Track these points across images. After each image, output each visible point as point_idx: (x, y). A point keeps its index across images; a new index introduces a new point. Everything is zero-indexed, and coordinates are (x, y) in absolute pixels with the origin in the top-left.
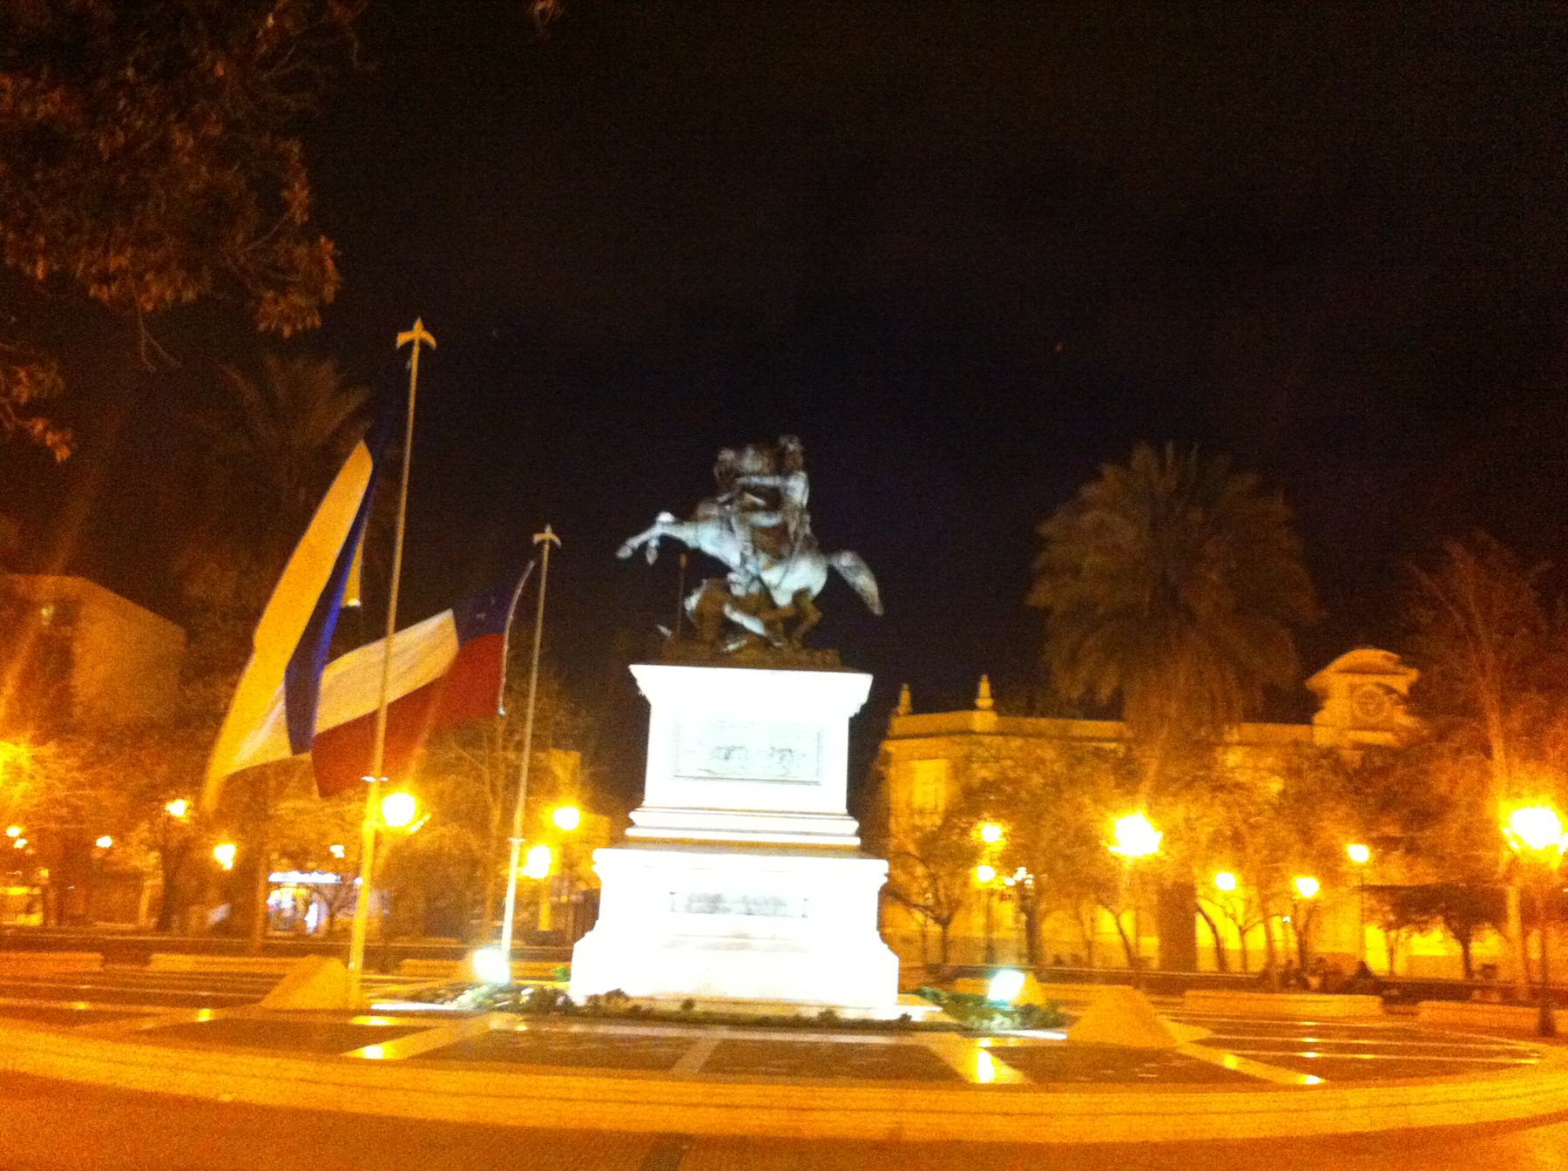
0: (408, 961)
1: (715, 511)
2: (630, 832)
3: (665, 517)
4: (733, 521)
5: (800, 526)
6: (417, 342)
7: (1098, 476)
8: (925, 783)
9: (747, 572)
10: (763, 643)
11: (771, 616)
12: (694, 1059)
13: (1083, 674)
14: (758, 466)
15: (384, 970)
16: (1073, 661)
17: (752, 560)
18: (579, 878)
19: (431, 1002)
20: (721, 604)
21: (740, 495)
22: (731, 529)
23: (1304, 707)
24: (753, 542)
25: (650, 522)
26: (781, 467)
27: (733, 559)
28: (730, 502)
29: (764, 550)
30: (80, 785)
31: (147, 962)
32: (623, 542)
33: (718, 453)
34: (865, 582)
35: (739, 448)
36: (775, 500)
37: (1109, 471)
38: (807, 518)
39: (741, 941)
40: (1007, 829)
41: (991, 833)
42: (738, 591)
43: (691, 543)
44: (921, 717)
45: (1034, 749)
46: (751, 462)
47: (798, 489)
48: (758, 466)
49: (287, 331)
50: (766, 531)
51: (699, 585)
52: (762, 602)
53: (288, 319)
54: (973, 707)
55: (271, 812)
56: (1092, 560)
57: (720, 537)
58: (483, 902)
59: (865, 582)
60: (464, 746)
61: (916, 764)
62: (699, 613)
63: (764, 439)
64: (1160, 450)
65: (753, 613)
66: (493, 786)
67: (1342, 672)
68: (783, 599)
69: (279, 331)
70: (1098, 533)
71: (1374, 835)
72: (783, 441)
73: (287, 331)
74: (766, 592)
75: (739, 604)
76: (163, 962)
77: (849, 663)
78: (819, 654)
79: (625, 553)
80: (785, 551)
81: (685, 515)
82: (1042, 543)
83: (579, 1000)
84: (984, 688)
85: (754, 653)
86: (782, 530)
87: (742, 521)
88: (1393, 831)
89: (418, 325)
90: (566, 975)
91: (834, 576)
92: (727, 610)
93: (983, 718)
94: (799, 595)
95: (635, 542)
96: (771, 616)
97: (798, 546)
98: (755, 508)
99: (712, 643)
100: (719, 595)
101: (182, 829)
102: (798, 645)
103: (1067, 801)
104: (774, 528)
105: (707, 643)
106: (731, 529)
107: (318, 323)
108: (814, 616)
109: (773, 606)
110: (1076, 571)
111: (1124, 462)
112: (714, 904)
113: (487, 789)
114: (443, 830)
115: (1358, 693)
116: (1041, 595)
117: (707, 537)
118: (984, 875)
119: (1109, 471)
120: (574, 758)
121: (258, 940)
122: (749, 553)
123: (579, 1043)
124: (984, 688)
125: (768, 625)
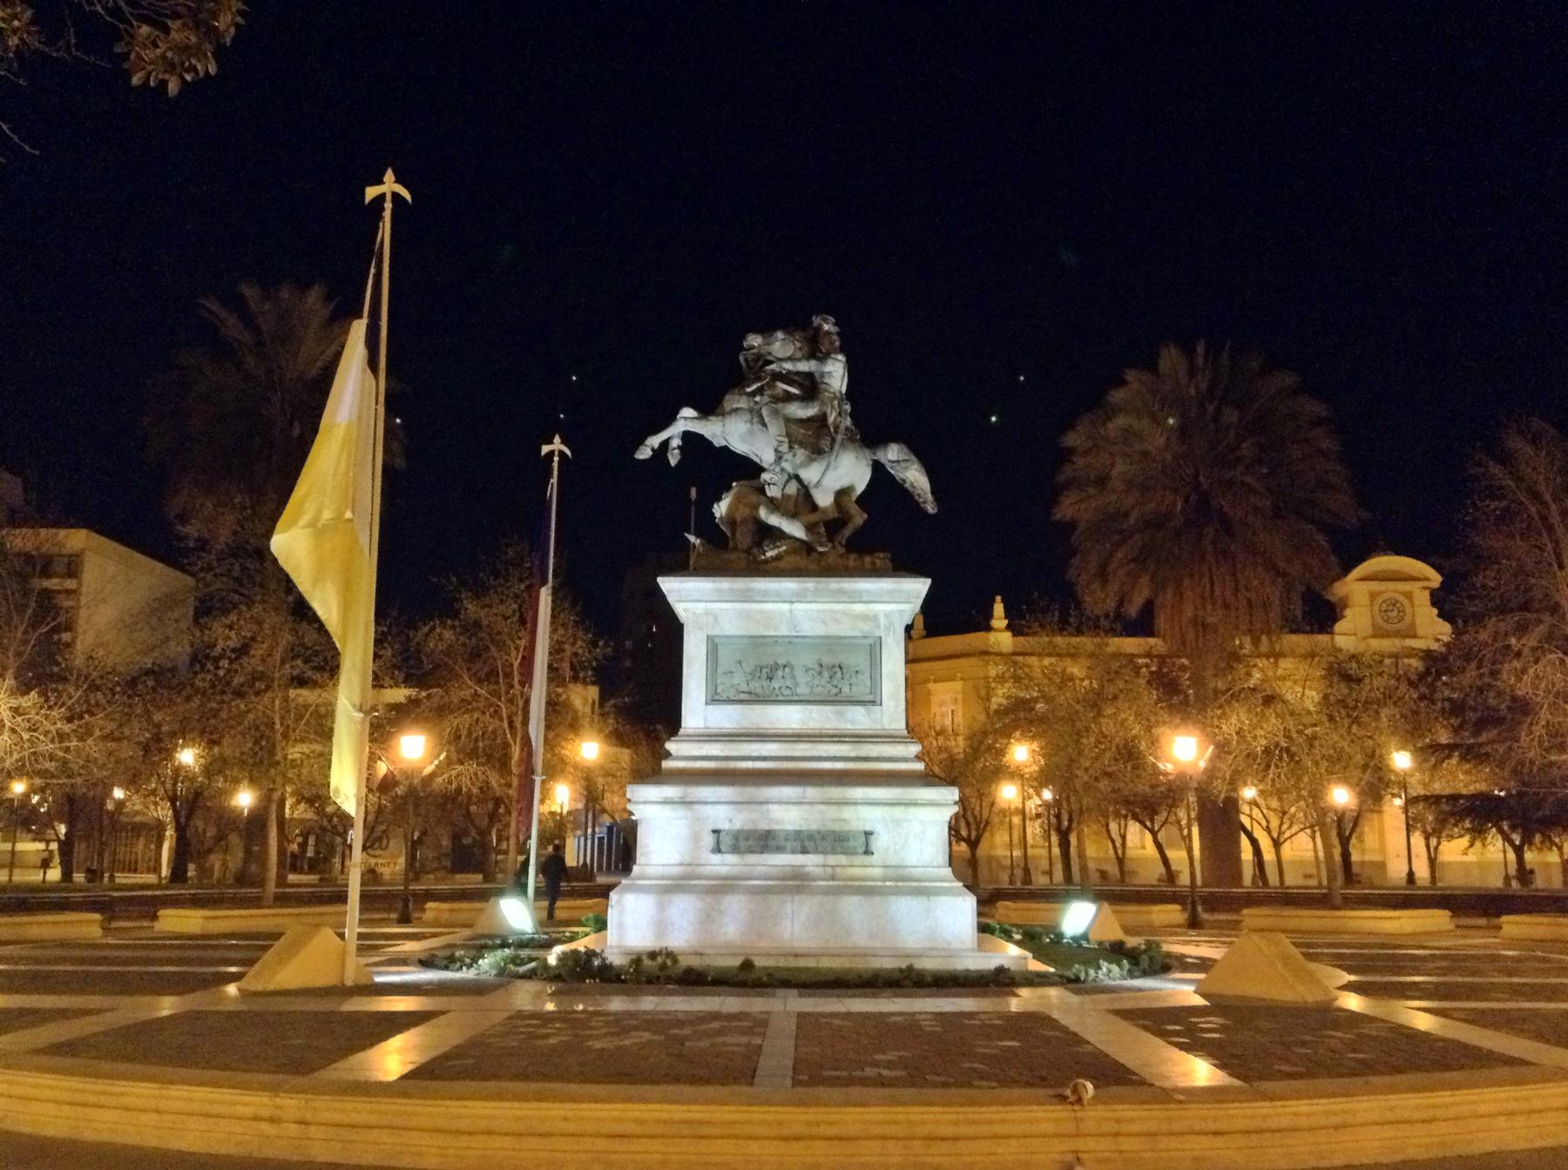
0: (430, 905)
1: (742, 403)
2: (666, 764)
3: (688, 412)
4: (765, 412)
5: (839, 417)
6: (389, 197)
7: (1122, 383)
8: (941, 705)
9: (783, 470)
10: (807, 548)
11: (813, 518)
12: (779, 1052)
13: (1114, 587)
14: (789, 350)
15: (405, 920)
16: (1103, 574)
17: (789, 456)
18: (604, 811)
19: (446, 968)
20: (756, 507)
21: (771, 385)
22: (764, 425)
23: (1323, 615)
24: (788, 435)
25: (670, 419)
26: (815, 351)
27: (765, 456)
28: (760, 391)
29: (801, 444)
30: (62, 736)
31: (155, 917)
32: (641, 441)
33: (743, 338)
34: (915, 477)
35: (766, 330)
36: (811, 387)
37: (1131, 375)
38: (848, 407)
39: (797, 883)
40: (1035, 746)
41: (1021, 753)
42: (773, 492)
43: (718, 442)
44: (936, 640)
45: (1070, 662)
46: (782, 348)
47: (836, 374)
48: (789, 350)
49: (173, 87)
50: (802, 422)
51: (729, 488)
52: (802, 504)
53: (171, 67)
54: (989, 629)
55: (279, 757)
56: (1120, 467)
57: (751, 432)
58: (508, 839)
59: (915, 477)
60: (480, 682)
61: (931, 686)
62: (731, 521)
63: (795, 321)
64: (1190, 353)
65: (793, 515)
66: (511, 723)
67: (1362, 579)
68: (824, 499)
69: (163, 84)
70: (1128, 442)
71: (1419, 745)
72: (816, 321)
73: (173, 87)
74: (805, 493)
75: (774, 505)
76: (174, 921)
77: (903, 567)
78: (868, 559)
79: (644, 453)
80: (825, 443)
81: (709, 408)
82: (1067, 454)
83: (616, 959)
84: (999, 608)
85: (796, 560)
86: (821, 420)
87: (775, 413)
88: (1444, 738)
89: (389, 176)
90: (601, 925)
91: (878, 469)
92: (763, 513)
93: (1001, 637)
94: (842, 494)
95: (655, 441)
96: (813, 518)
97: (839, 438)
98: (788, 398)
99: (748, 551)
100: (753, 498)
101: (193, 779)
102: (842, 550)
103: (1109, 717)
104: (810, 420)
105: (742, 553)
106: (764, 425)
107: (212, 70)
108: (859, 518)
109: (814, 507)
110: (1102, 482)
111: (1150, 365)
112: (764, 841)
113: (506, 724)
114: (460, 768)
115: (1379, 600)
116: (1067, 508)
117: (733, 432)
118: (1008, 793)
119: (1131, 375)
120: (593, 692)
121: (271, 888)
122: (784, 448)
123: (625, 1031)
124: (999, 608)
125: (809, 528)
